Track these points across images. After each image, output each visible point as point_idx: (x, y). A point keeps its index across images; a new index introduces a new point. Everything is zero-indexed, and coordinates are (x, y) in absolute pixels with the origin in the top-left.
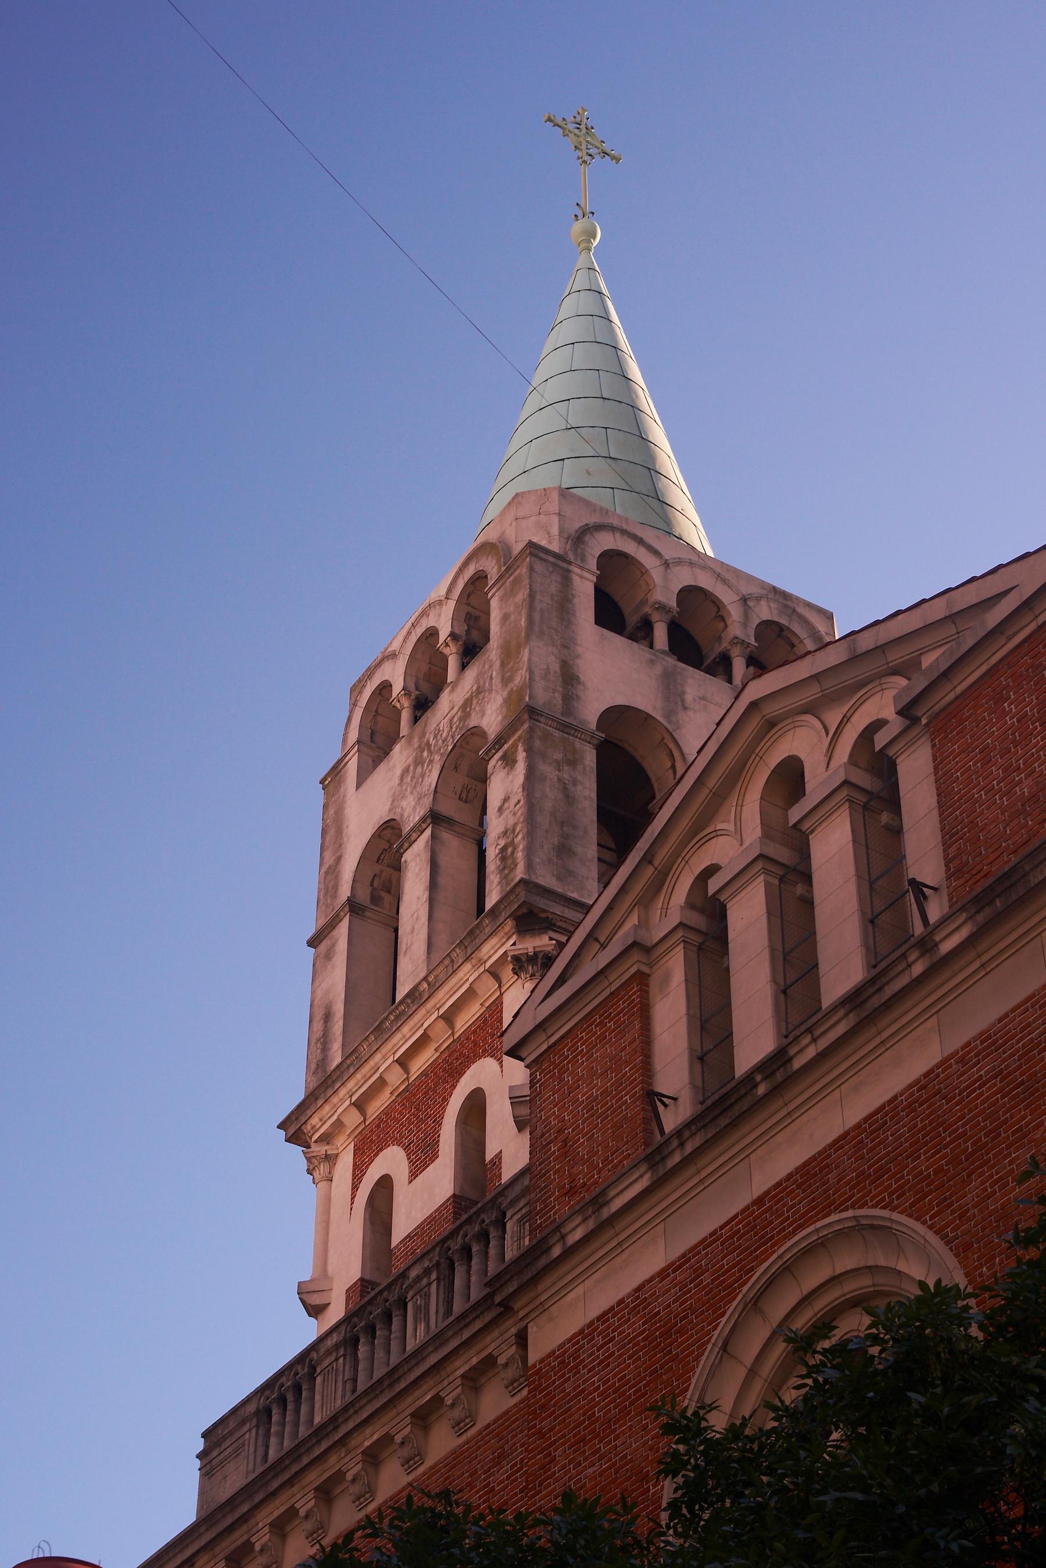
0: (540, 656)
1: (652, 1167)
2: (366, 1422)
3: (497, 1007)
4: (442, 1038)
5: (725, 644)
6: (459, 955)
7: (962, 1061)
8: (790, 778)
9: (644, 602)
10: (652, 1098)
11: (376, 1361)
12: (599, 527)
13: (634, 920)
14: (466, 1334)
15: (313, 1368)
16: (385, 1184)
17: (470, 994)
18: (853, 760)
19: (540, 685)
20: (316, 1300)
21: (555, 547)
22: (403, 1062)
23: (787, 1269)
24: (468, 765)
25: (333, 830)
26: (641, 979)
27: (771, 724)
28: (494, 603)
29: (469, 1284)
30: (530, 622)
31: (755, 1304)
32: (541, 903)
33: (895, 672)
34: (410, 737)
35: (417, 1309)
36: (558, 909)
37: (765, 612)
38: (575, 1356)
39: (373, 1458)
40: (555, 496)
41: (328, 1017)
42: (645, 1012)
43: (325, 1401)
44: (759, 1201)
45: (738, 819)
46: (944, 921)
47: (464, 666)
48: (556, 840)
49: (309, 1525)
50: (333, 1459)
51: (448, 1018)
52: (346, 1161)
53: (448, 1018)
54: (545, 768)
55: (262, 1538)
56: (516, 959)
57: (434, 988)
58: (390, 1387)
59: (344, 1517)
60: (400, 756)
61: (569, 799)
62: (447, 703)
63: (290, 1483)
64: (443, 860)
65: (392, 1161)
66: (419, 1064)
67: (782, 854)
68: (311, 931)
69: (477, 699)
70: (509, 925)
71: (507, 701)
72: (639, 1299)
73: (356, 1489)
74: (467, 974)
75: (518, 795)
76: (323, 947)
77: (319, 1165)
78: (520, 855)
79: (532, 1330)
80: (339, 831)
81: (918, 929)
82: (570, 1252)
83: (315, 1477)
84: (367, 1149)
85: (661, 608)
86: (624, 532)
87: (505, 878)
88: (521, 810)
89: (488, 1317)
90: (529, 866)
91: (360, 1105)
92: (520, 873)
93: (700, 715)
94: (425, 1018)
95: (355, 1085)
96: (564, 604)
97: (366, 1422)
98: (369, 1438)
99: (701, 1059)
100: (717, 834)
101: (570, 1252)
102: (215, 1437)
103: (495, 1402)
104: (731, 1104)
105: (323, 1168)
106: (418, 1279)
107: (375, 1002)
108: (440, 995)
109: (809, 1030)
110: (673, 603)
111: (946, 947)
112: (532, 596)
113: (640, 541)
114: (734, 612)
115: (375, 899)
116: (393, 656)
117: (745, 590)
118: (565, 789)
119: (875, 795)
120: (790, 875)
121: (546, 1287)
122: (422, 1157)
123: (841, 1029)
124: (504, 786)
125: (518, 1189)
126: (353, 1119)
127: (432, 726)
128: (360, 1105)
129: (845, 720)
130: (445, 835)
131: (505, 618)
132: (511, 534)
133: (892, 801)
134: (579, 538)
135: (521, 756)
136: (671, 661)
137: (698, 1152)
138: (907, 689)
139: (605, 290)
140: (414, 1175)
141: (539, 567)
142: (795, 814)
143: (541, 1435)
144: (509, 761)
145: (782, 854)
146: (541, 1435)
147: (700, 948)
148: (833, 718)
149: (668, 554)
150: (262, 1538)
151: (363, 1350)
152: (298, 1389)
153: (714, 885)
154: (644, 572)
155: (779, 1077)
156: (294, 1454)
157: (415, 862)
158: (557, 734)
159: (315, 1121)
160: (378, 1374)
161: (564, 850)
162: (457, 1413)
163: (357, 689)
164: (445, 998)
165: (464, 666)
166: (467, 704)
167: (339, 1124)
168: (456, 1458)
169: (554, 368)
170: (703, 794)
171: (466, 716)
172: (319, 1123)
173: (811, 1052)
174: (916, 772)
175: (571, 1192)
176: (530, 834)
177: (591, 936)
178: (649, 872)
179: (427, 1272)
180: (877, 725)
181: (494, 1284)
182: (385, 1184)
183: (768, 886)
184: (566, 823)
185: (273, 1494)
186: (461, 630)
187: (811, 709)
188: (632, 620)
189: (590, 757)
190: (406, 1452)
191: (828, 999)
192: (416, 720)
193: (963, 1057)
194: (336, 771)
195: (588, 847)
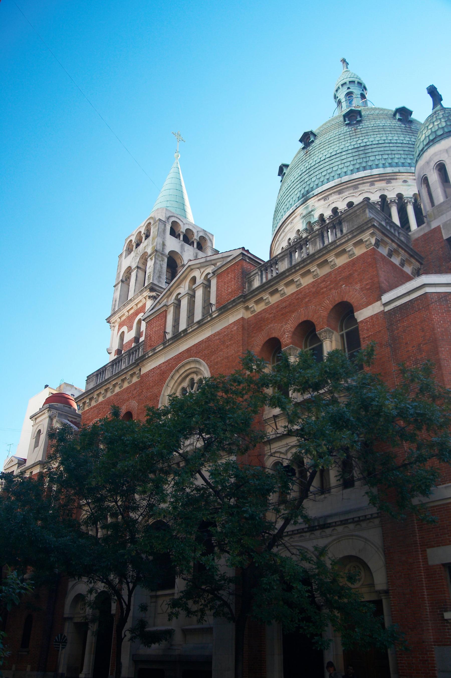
0: (159, 240)
1: (164, 345)
2: (114, 380)
3: (145, 305)
4: (135, 308)
5: (193, 240)
6: (139, 294)
7: (214, 336)
8: (194, 280)
9: (179, 231)
10: (165, 332)
11: (117, 370)
12: (172, 216)
13: (165, 300)
14: (131, 368)
15: (106, 369)
16: (123, 332)
17: (141, 301)
18: (204, 279)
19: (158, 246)
20: (110, 352)
21: (164, 220)
22: (128, 311)
23: (183, 366)
24: (144, 258)
25: (120, 266)
26: (166, 311)
27: (192, 269)
28: (152, 229)
29: (132, 361)
30: (158, 234)
31: (177, 371)
32: (154, 287)
33: (213, 265)
34: (135, 251)
35: (124, 361)
36: (157, 288)
37: (201, 234)
38: (148, 374)
39: (114, 386)
40: (165, 210)
41: (116, 301)
42: (166, 317)
43: (107, 375)
44: (180, 353)
45: (185, 285)
46: (215, 311)
47: (146, 239)
48: (158, 275)
49: (103, 395)
50: (108, 385)
51: (137, 305)
52: (117, 327)
53: (137, 305)
54: (157, 261)
55: (95, 396)
56: (149, 296)
57: (134, 299)
58: (118, 375)
59: (109, 395)
60: (133, 254)
61: (161, 267)
62: (142, 246)
63: (100, 388)
64: (138, 275)
65: (125, 329)
66: (131, 312)
67: (191, 293)
68: (114, 285)
69: (147, 246)
70: (148, 290)
71: (152, 248)
72: (159, 367)
73: (111, 391)
74: (140, 298)
75: (152, 266)
76: (116, 287)
77: (113, 327)
78: (151, 277)
79: (142, 369)
80: (121, 266)
81: (211, 312)
82: (149, 357)
83: (105, 388)
84: (121, 325)
85: (182, 232)
86: (177, 217)
87: (149, 281)
88: (153, 269)
89: (135, 366)
90: (153, 280)
91: (120, 318)
92: (151, 281)
93: (188, 254)
94: (132, 304)
95: (120, 314)
96: (164, 230)
97: (114, 380)
98: (114, 382)
99: (174, 327)
100: (181, 287)
101: (149, 357)
102: (89, 378)
103: (135, 380)
104: (178, 336)
105: (113, 328)
106: (124, 356)
107: (124, 299)
108: (135, 301)
109: (191, 326)
110: (184, 232)
111: (214, 316)
112: (158, 229)
113: (180, 219)
114: (195, 234)
115: (126, 280)
116: (133, 235)
117: (198, 230)
118: (161, 265)
119: (207, 286)
120: (192, 297)
121: (145, 362)
122: (130, 328)
123: (196, 327)
124: (150, 263)
125: (142, 344)
126: (119, 320)
127: (139, 250)
128: (120, 318)
129: (204, 271)
130: (139, 271)
131: (153, 232)
132: (156, 216)
133: (209, 286)
134: (168, 218)
135: (154, 259)
136: (183, 242)
137: (171, 344)
138: (214, 269)
139: (179, 168)
140: (128, 332)
141: (160, 223)
142: (194, 287)
143: (141, 387)
144: (151, 259)
145: (191, 293)
146: (141, 387)
147: (176, 307)
148: (202, 270)
149: (184, 222)
150: (95, 396)
151: (114, 367)
152: (103, 372)
153: (179, 297)
154: (180, 225)
155: (185, 333)
156: (101, 383)
157: (133, 274)
158: (160, 255)
159: (112, 320)
160: (117, 372)
161: (160, 277)
162: (129, 381)
163: (126, 240)
164: (136, 301)
165: (146, 239)
166: (145, 247)
167: (116, 321)
168: (128, 388)
169: (168, 184)
170: (179, 280)
171: (145, 249)
172: (112, 320)
173: (191, 330)
174: (214, 282)
175: (150, 346)
176: (154, 274)
177: (158, 302)
178: (169, 292)
179: (126, 355)
180: (208, 274)
181: (136, 360)
182: (123, 332)
183: (188, 298)
184: (160, 272)
185: (97, 390)
186: (146, 232)
187: (198, 268)
188: (177, 234)
189: (166, 260)
190: (120, 386)
191: (195, 321)
192: (136, 248)
193: (215, 335)
194: (121, 255)
195: (164, 277)
